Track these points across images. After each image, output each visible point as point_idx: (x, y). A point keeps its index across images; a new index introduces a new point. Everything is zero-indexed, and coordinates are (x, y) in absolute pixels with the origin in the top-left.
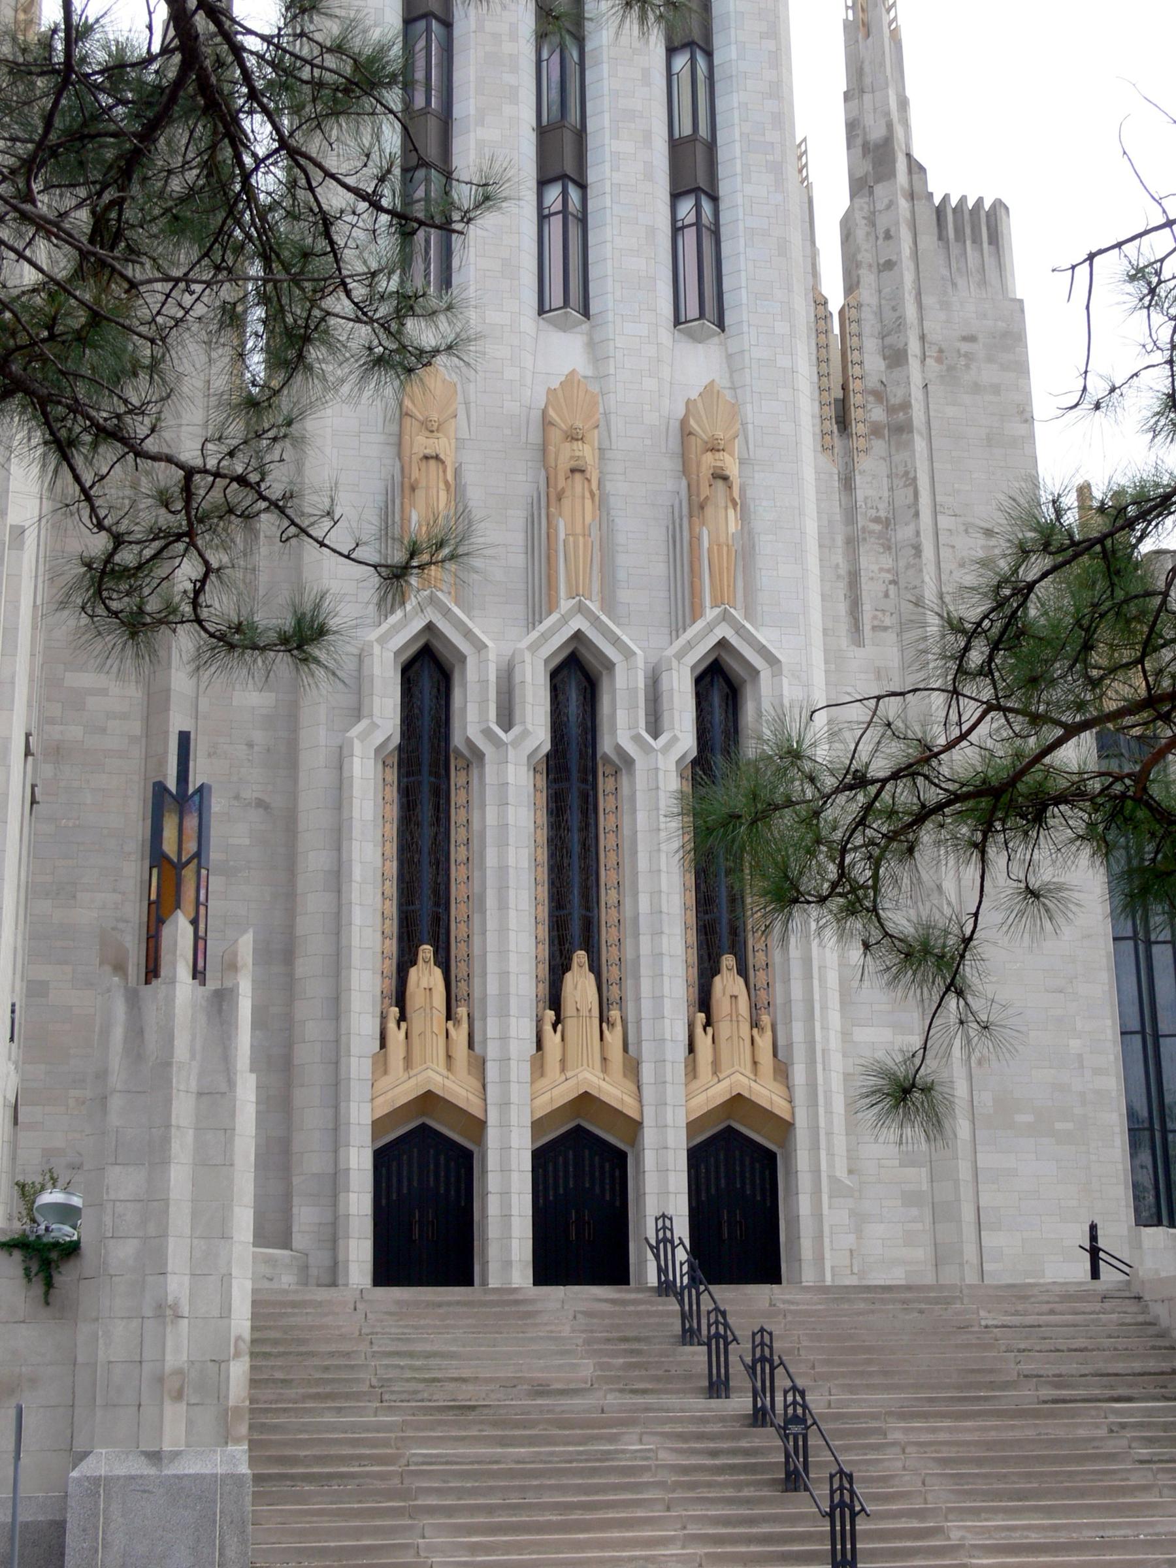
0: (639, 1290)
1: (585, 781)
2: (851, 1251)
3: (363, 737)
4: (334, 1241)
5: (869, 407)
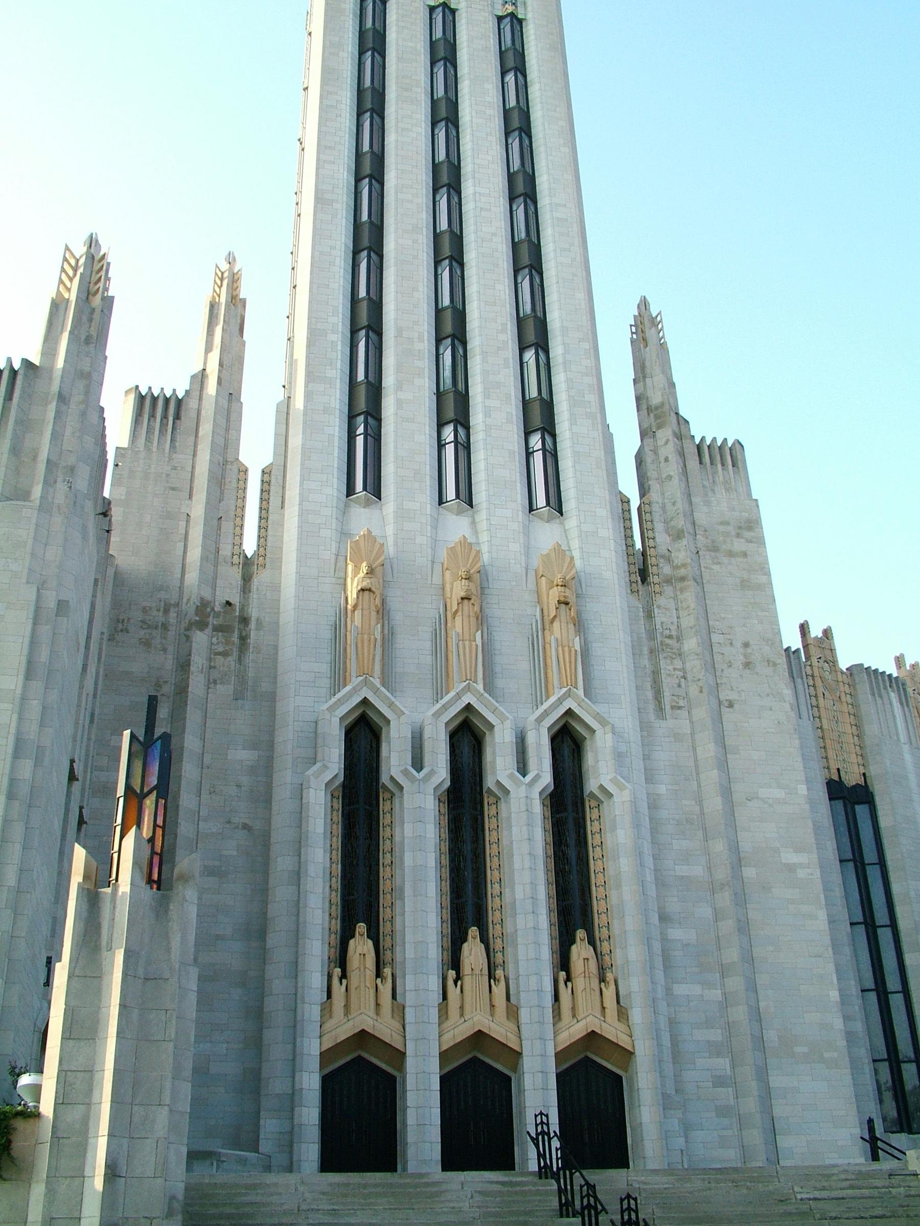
0: (522, 1174)
1: (476, 809)
2: (682, 1151)
3: (317, 775)
4: (291, 1145)
5: (661, 565)
